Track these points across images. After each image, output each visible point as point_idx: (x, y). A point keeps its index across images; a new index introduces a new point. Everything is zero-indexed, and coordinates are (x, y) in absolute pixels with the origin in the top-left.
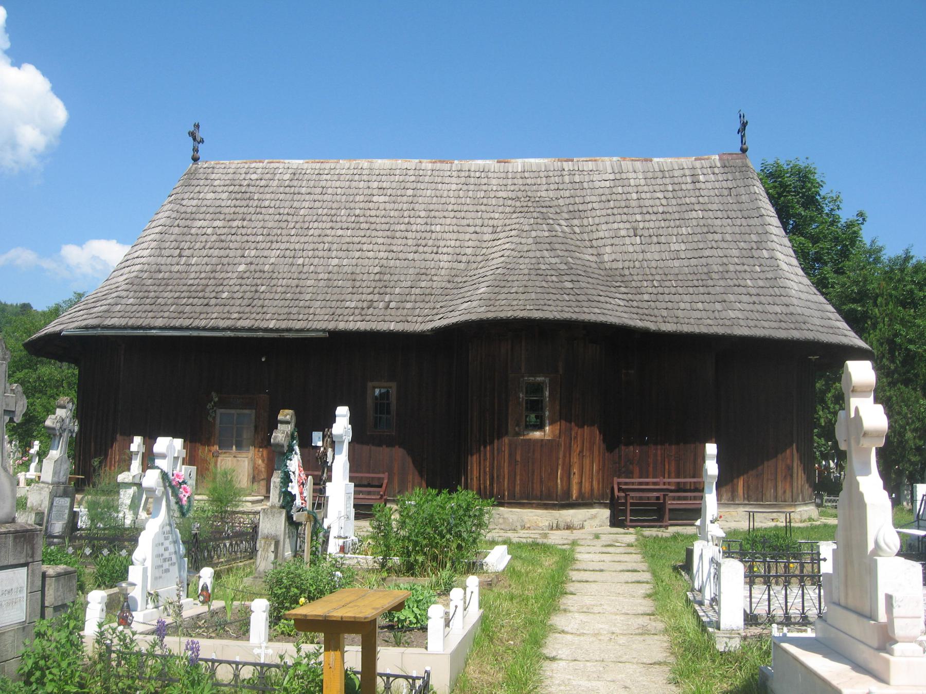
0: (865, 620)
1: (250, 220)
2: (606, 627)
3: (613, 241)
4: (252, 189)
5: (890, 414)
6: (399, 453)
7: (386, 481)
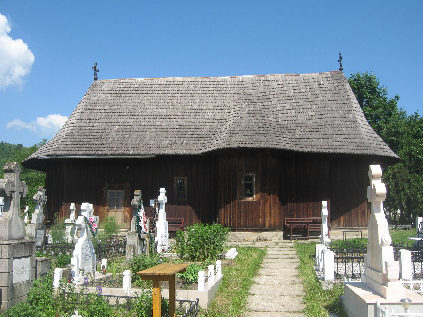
0: (378, 273)
1: (121, 106)
2: (277, 281)
3: (282, 112)
4: (121, 92)
5: (387, 187)
6: (189, 208)
7: (183, 221)
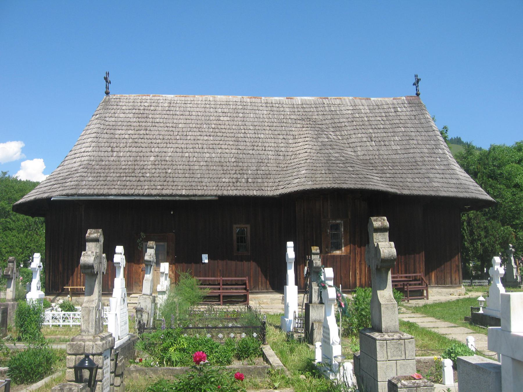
1: (150, 130)
3: (360, 144)
4: (146, 112)
6: (253, 265)
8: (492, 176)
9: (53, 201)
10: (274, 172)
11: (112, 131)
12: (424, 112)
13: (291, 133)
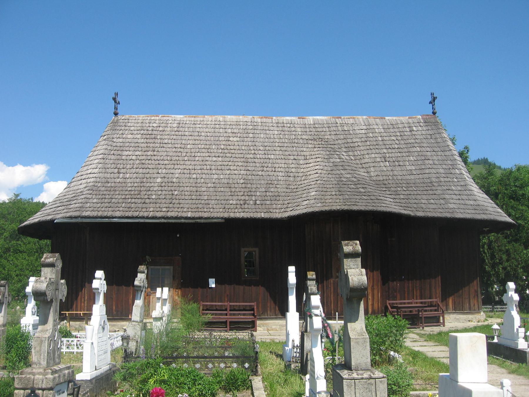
1: (158, 151)
6: (261, 290)
8: (514, 197)
9: (57, 223)
10: (283, 194)
11: (119, 152)
12: (440, 131)
13: (302, 153)
